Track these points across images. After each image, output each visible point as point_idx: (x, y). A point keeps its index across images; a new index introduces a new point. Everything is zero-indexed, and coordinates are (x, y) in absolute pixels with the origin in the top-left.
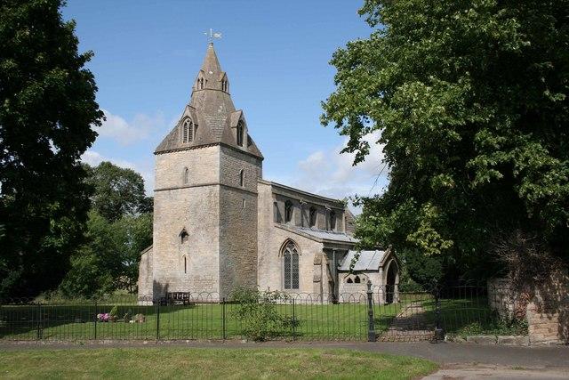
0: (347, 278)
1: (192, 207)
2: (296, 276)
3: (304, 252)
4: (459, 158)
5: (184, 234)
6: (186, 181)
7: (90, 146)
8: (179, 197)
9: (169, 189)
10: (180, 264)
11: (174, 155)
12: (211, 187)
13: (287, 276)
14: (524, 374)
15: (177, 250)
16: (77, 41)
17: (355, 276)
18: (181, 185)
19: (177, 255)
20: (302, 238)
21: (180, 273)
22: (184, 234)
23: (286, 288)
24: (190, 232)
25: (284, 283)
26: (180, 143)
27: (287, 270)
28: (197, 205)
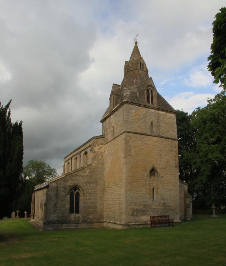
21: (150, 202)
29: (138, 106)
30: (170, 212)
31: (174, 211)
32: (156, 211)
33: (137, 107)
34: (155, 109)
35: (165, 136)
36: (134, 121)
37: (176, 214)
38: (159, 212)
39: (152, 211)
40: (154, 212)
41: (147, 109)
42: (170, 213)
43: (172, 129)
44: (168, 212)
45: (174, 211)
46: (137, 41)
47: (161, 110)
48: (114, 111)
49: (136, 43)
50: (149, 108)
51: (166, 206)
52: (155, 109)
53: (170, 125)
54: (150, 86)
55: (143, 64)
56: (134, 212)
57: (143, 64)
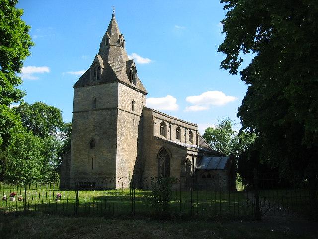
3: (174, 156)
5: (92, 144)
6: (94, 107)
9: (83, 111)
12: (112, 110)
24: (97, 140)
48: (206, 174)
54: (133, 67)
55: (123, 42)
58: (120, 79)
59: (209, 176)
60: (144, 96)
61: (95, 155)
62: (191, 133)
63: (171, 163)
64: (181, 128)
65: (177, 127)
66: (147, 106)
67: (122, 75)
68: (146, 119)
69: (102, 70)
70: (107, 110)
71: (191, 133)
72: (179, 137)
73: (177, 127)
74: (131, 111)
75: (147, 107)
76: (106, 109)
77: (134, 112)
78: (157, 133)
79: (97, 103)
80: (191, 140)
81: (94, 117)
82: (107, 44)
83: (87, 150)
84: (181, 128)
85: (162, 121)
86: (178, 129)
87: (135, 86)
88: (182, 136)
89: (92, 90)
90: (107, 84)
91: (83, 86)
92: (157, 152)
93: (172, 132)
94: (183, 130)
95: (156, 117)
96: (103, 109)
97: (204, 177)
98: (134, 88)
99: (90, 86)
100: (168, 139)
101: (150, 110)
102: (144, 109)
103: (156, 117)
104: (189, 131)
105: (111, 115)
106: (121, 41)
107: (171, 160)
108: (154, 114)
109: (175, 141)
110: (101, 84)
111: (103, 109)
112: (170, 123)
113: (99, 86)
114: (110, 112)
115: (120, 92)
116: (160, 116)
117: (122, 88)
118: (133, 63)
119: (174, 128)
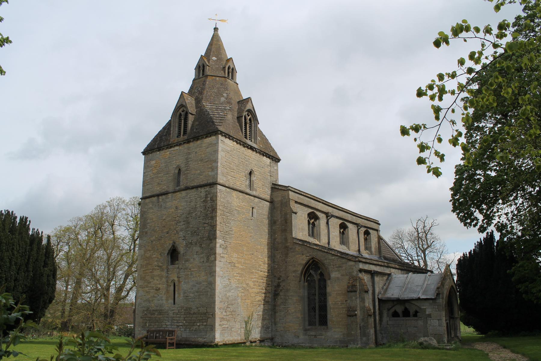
0: (392, 311)
1: (184, 216)
2: (323, 308)
3: (334, 275)
4: (499, 126)
5: (174, 254)
6: (178, 183)
7: (452, 189)
8: (169, 204)
9: (158, 195)
10: (168, 291)
11: (167, 153)
12: (207, 189)
13: (311, 309)
14: (200, 357)
15: (164, 274)
16: (515, 18)
17: (403, 308)
18: (171, 189)
19: (164, 280)
20: (330, 257)
21: (167, 304)
22: (174, 254)
23: (310, 324)
24: (181, 250)
25: (307, 318)
26: (173, 138)
27: (310, 301)
28: (190, 213)
29: (159, 151)
30: (198, 324)
31: (205, 324)
32: (176, 321)
33: (158, 153)
34: (182, 143)
35: (195, 184)
36: (153, 178)
37: (209, 329)
38: (181, 324)
39: (170, 321)
40: (173, 324)
41: (172, 149)
42: (199, 326)
43: (210, 166)
44: (195, 324)
45: (205, 324)
46: (217, 27)
47: (192, 140)
48: (399, 309)
49: (216, 29)
50: (175, 146)
51: (192, 313)
52: (182, 143)
53: (206, 160)
54: (249, 111)
55: (233, 69)
56: (146, 323)
57: (233, 69)
58: (221, 128)
59: (406, 313)
60: (273, 163)
61: (178, 277)
62: (367, 233)
63: (329, 289)
64: (371, 231)
65: (341, 221)
66: (282, 182)
67: (229, 121)
68: (280, 201)
69: (191, 118)
70: (199, 189)
71: (367, 233)
72: (344, 240)
73: (341, 221)
74: (248, 191)
75: (280, 183)
76: (197, 187)
77: (254, 193)
78: (300, 229)
79: (182, 177)
80: (368, 248)
81: (179, 203)
82: (203, 74)
83: (165, 267)
84: (371, 231)
85: (342, 221)
86: (343, 227)
87: (254, 145)
88: (351, 239)
89: (176, 156)
90: (199, 142)
91: (160, 149)
92: (300, 269)
93: (330, 229)
94: (352, 230)
95: (296, 202)
96: (193, 188)
97: (395, 314)
98: (252, 148)
99: (171, 147)
100: (323, 241)
101: (287, 189)
102: (275, 188)
103: (296, 202)
104: (363, 230)
105: (206, 197)
106: (229, 68)
107: (328, 282)
108: (292, 195)
109: (336, 245)
110: (188, 141)
111: (193, 188)
112: (327, 214)
113: (186, 146)
114: (203, 192)
115: (221, 155)
116: (306, 201)
117: (225, 145)
118: (250, 104)
119: (335, 223)
